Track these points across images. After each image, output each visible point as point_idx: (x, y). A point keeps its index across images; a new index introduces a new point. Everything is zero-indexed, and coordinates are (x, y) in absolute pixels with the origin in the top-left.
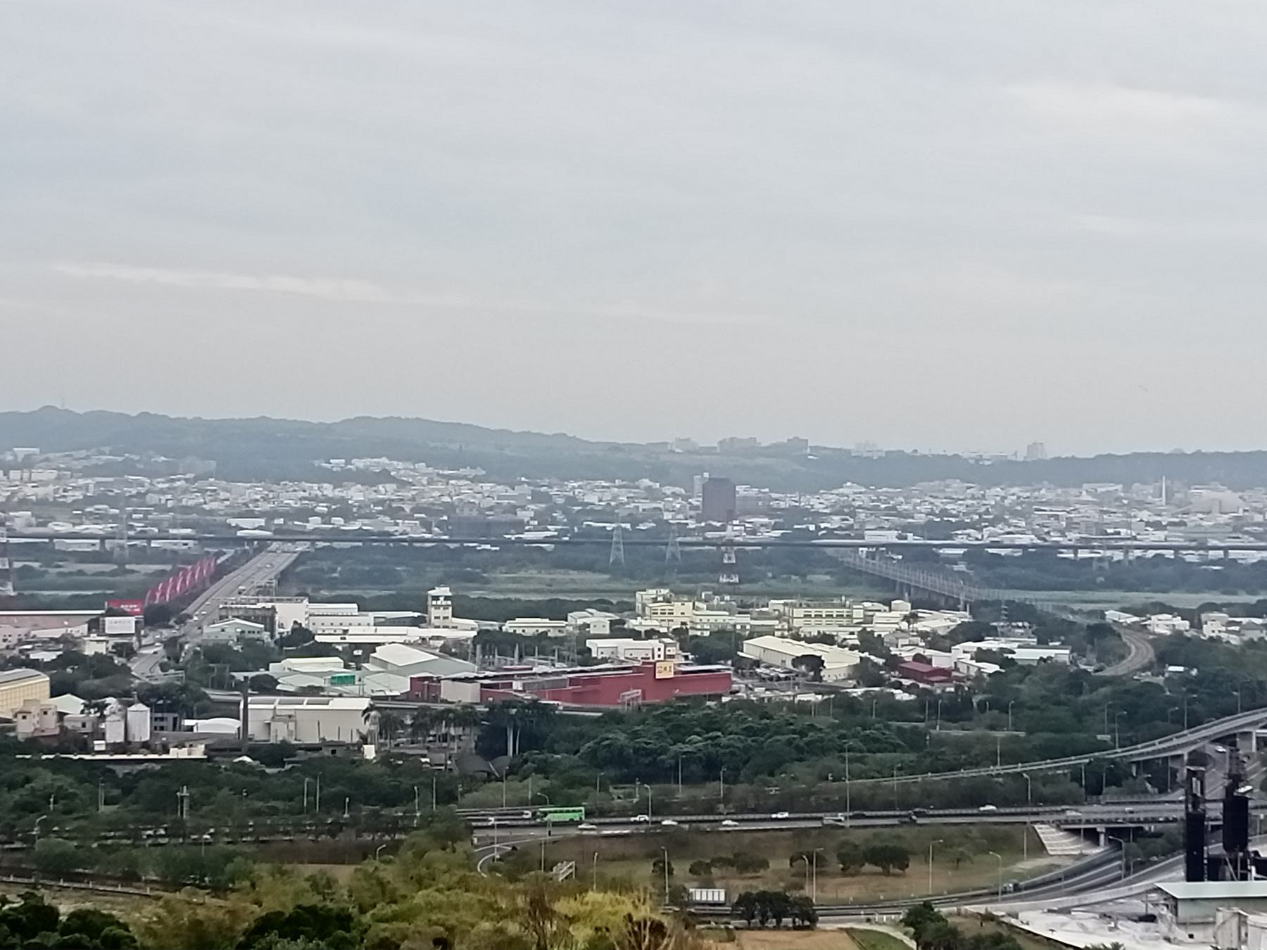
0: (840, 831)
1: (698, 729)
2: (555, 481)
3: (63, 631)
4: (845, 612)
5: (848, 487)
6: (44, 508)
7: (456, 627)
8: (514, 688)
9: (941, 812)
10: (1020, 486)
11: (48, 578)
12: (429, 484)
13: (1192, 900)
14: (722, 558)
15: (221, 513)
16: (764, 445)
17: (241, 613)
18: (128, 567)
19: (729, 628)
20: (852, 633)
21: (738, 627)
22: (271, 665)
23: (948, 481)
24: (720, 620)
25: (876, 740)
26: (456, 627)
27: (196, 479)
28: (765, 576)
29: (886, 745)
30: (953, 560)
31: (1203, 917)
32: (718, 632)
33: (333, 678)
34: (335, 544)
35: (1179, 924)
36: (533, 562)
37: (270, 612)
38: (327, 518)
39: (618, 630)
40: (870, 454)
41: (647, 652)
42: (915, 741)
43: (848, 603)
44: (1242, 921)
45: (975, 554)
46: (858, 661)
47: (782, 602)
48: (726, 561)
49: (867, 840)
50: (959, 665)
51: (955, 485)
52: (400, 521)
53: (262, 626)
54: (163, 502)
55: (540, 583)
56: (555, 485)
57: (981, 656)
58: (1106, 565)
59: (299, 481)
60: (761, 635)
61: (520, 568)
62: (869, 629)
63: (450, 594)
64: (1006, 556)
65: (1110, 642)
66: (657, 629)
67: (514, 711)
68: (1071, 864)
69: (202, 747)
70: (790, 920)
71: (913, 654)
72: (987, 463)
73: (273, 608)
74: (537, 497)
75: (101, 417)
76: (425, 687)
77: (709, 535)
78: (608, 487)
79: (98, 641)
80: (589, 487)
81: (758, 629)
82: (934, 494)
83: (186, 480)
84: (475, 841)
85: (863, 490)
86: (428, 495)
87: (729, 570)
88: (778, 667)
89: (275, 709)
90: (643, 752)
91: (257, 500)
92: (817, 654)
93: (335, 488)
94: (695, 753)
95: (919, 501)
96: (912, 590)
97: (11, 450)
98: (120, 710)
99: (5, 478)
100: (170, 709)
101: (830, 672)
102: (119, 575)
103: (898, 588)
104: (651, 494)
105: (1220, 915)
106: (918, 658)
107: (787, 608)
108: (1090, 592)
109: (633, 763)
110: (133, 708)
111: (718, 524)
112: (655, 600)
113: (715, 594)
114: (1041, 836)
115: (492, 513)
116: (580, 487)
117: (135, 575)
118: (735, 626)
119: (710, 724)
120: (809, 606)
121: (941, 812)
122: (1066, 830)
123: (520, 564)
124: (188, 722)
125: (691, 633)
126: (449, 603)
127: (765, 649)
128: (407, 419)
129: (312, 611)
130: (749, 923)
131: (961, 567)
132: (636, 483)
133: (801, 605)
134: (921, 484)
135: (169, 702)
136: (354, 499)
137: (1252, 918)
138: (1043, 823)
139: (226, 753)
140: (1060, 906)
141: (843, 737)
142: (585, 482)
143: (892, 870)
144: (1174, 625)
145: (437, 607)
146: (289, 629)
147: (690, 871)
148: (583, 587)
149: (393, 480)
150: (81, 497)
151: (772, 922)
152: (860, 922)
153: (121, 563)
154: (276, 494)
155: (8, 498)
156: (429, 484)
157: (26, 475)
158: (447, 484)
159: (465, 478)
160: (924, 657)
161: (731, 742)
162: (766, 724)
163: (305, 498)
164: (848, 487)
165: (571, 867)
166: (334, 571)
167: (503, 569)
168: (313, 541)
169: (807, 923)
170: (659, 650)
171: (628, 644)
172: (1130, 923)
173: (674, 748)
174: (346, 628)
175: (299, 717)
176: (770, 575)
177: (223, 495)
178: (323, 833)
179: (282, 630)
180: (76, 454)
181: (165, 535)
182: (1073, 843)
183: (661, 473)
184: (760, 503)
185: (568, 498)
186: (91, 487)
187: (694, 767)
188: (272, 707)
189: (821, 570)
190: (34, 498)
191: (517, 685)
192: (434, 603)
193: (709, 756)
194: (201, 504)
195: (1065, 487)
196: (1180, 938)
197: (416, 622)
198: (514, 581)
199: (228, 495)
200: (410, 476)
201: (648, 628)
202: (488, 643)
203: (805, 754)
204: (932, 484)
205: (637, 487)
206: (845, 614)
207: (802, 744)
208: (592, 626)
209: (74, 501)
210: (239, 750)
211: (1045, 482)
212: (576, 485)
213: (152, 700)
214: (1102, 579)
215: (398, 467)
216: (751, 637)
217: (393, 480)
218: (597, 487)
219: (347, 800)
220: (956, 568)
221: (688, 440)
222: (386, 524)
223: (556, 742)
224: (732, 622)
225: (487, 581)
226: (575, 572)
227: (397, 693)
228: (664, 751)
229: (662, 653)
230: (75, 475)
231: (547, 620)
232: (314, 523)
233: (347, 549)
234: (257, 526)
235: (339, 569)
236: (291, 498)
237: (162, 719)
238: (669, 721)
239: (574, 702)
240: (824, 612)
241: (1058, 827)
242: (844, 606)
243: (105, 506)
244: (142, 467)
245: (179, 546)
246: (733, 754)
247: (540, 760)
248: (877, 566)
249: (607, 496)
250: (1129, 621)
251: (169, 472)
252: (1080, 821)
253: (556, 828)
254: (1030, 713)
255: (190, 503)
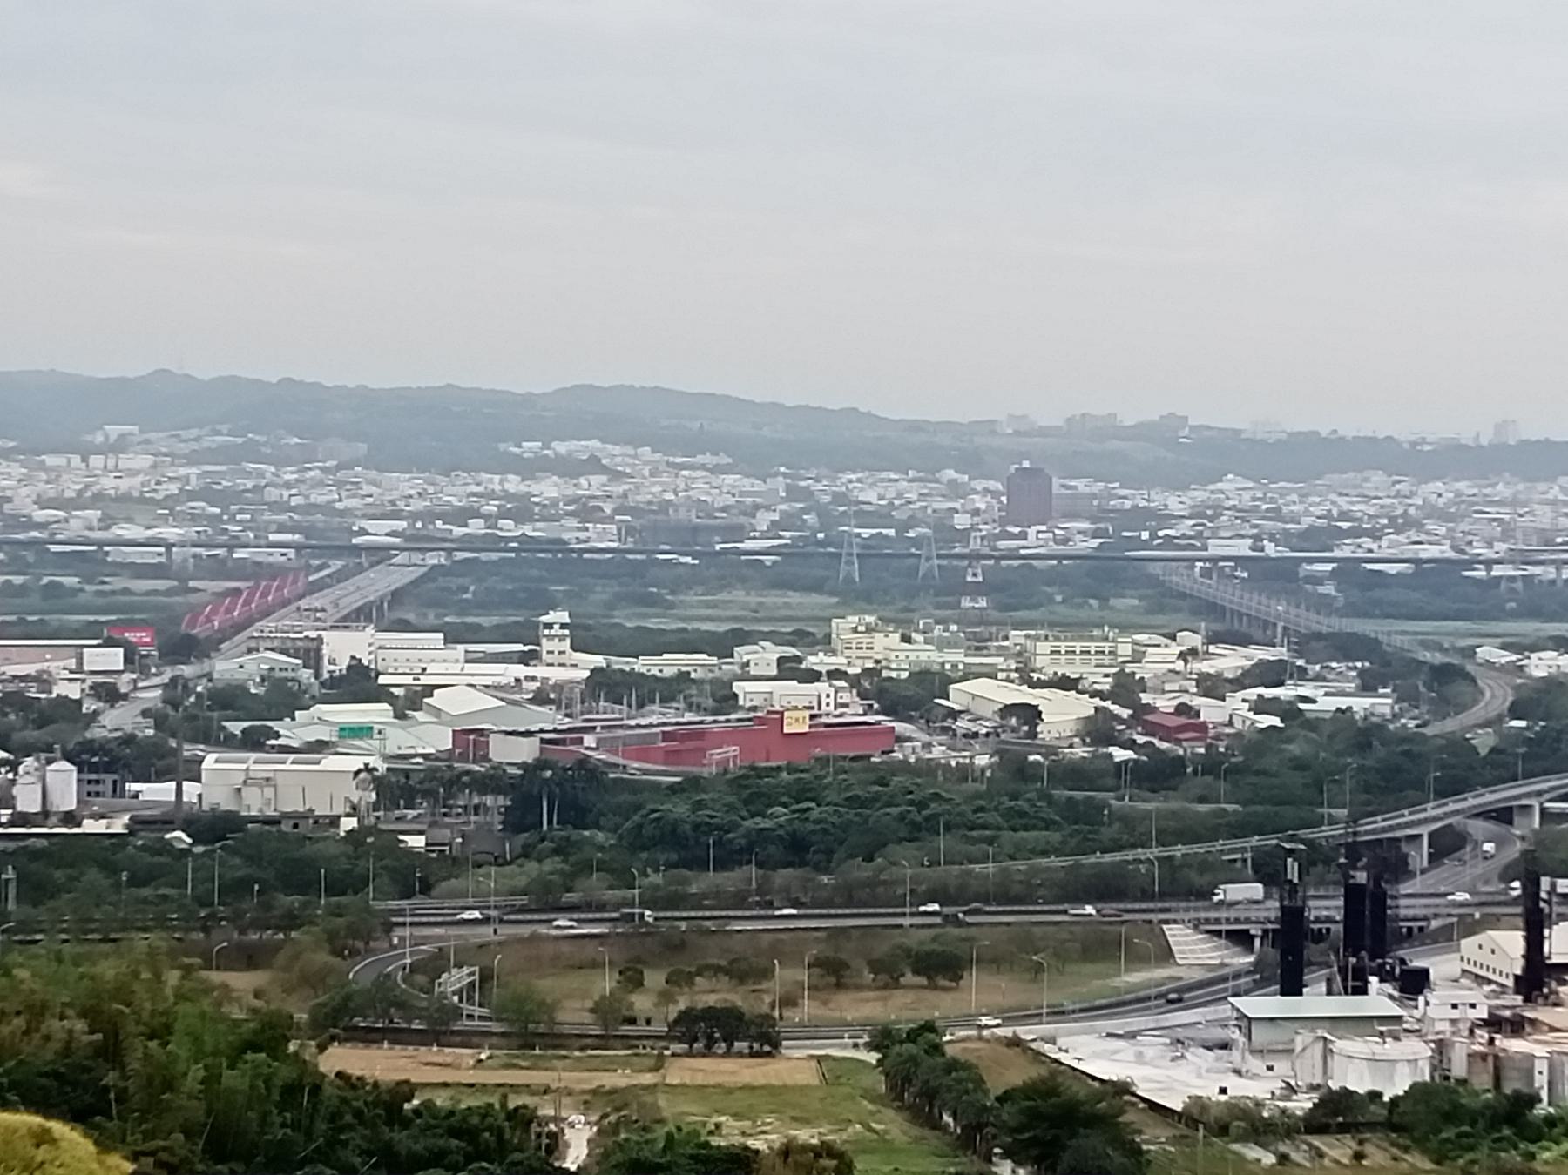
0: (899, 931)
1: (785, 799)
2: (824, 471)
3: (39, 666)
4: (1107, 647)
5: (1230, 481)
6: (117, 506)
7: (576, 665)
8: (586, 744)
9: (1053, 907)
10: (1469, 479)
11: (82, 597)
12: (652, 475)
13: (1272, 1019)
14: (965, 577)
15: (359, 513)
16: (1128, 423)
17: (276, 644)
18: (191, 584)
19: (936, 667)
20: (1107, 676)
21: (948, 666)
22: (297, 713)
23: (1366, 474)
24: (923, 656)
25: (1022, 814)
26: (576, 665)
27: (338, 468)
28: (1051, 600)
29: (1034, 821)
30: (1317, 580)
31: (1284, 1043)
32: (920, 673)
33: (342, 729)
34: (483, 556)
35: (1252, 1052)
36: (743, 580)
37: (315, 644)
38: (493, 520)
39: (789, 670)
40: (1267, 436)
41: (810, 698)
42: (1088, 815)
43: (1111, 634)
44: (1327, 1052)
45: (1347, 571)
46: (1092, 712)
47: (1024, 633)
48: (969, 579)
49: (922, 943)
50: (1235, 719)
51: (1374, 478)
52: (590, 525)
53: (299, 662)
54: (285, 498)
55: (743, 609)
56: (825, 477)
57: (1260, 706)
58: (1519, 585)
59: (477, 471)
60: (978, 676)
61: (722, 588)
62: (1127, 670)
63: (568, 620)
64: (1399, 574)
65: (1462, 687)
66: (843, 668)
67: (548, 773)
68: (1199, 975)
69: (126, 819)
70: (746, 1044)
71: (1176, 702)
72: (1427, 448)
73: (320, 639)
74: (793, 493)
75: (230, 383)
76: (471, 740)
77: (1002, 544)
78: (897, 480)
79: (70, 680)
80: (870, 481)
81: (974, 669)
82: (1345, 491)
83: (322, 469)
84: (396, 941)
85: (1251, 484)
86: (646, 490)
87: (976, 590)
88: (987, 720)
89: (247, 769)
90: (706, 829)
91: (411, 497)
92: (1034, 703)
93: (523, 480)
94: (774, 830)
95: (1317, 499)
96: (1245, 618)
97: (101, 428)
98: (36, 769)
99: (84, 465)
100: (107, 768)
101: (1049, 727)
102: (177, 595)
103: (1228, 616)
104: (956, 491)
105: (1299, 1039)
106: (1182, 709)
107: (1028, 642)
108: (1494, 623)
109: (692, 842)
110: (53, 766)
111: (1016, 530)
112: (855, 630)
113: (937, 623)
114: (1167, 933)
115: (724, 515)
116: (859, 480)
117: (199, 594)
118: (943, 664)
119: (804, 792)
120: (1057, 639)
121: (1053, 907)
122: (1208, 932)
123: (724, 584)
124: (133, 787)
125: (885, 674)
126: (567, 632)
127: (974, 696)
128: (643, 388)
129: (382, 643)
130: (691, 1047)
131: (1328, 589)
132: (937, 475)
133: (1046, 638)
134: (1328, 476)
135: (106, 759)
136: (546, 495)
137: (1339, 1045)
138: (1175, 922)
139: (153, 827)
140: (1128, 1029)
141: (981, 809)
142: (867, 473)
143: (942, 982)
144: (1559, 666)
145: (550, 637)
146: (344, 666)
147: (667, 982)
148: (799, 614)
149: (604, 470)
150: (176, 492)
151: (721, 1047)
152: (845, 1047)
153: (183, 580)
154: (438, 488)
155: (80, 493)
156: (652, 475)
157: (111, 463)
158: (677, 475)
159: (703, 467)
160: (1191, 708)
161: (824, 815)
162: (877, 792)
163: (474, 494)
164: (1230, 481)
165: (472, 974)
166: (466, 590)
167: (700, 590)
168: (449, 551)
169: (767, 1048)
170: (828, 696)
171: (788, 688)
172: (1202, 1050)
173: (746, 823)
174: (424, 665)
175: (280, 780)
176: (1059, 598)
177: (367, 489)
178: (194, 929)
179: (332, 668)
180: (183, 434)
181: (263, 542)
182: (1217, 949)
183: (973, 463)
184: (1095, 503)
185: (835, 495)
186: (193, 479)
187: (772, 849)
188: (244, 766)
189: (1133, 592)
190: (112, 492)
191: (589, 740)
192: (546, 632)
193: (793, 834)
194: (334, 501)
195: (1530, 480)
196: (1255, 1071)
197: (526, 659)
198: (708, 605)
199: (373, 489)
200: (628, 465)
201: (832, 668)
202: (603, 685)
203: (924, 832)
204: (1345, 476)
205: (937, 481)
206: (1107, 650)
207: (919, 819)
208: (752, 664)
209: (167, 497)
210: (171, 822)
211: (1507, 475)
212: (853, 477)
213: (85, 757)
214: (1513, 605)
215: (612, 454)
216: (964, 679)
217: (604, 470)
218: (882, 480)
219: (256, 887)
220: (1321, 589)
221: (1024, 417)
222: (569, 531)
223: (604, 815)
224: (941, 660)
225: (672, 606)
226: (797, 594)
227: (432, 751)
228: (733, 827)
229: (831, 700)
230: (176, 462)
231: (704, 656)
232: (476, 526)
233: (494, 562)
234: (388, 530)
235: (472, 588)
236: (454, 494)
237: (98, 782)
238: (746, 787)
239: (665, 764)
240: (1078, 646)
241: (1196, 927)
242: (1106, 639)
243: (202, 504)
244: (269, 451)
245: (276, 557)
246: (825, 831)
247: (561, 838)
248: (1212, 589)
249: (891, 494)
250: (1503, 661)
251: (302, 459)
252: (412, 924)
253: (502, 926)
254: (1254, 779)
255: (321, 500)
